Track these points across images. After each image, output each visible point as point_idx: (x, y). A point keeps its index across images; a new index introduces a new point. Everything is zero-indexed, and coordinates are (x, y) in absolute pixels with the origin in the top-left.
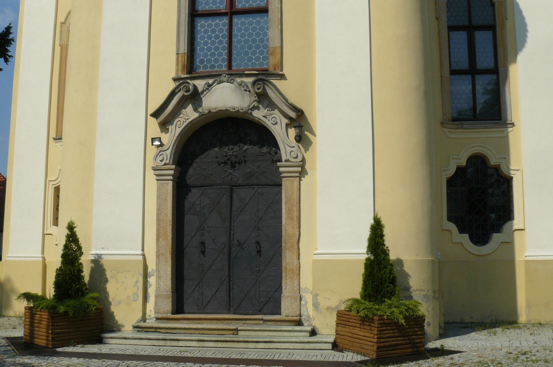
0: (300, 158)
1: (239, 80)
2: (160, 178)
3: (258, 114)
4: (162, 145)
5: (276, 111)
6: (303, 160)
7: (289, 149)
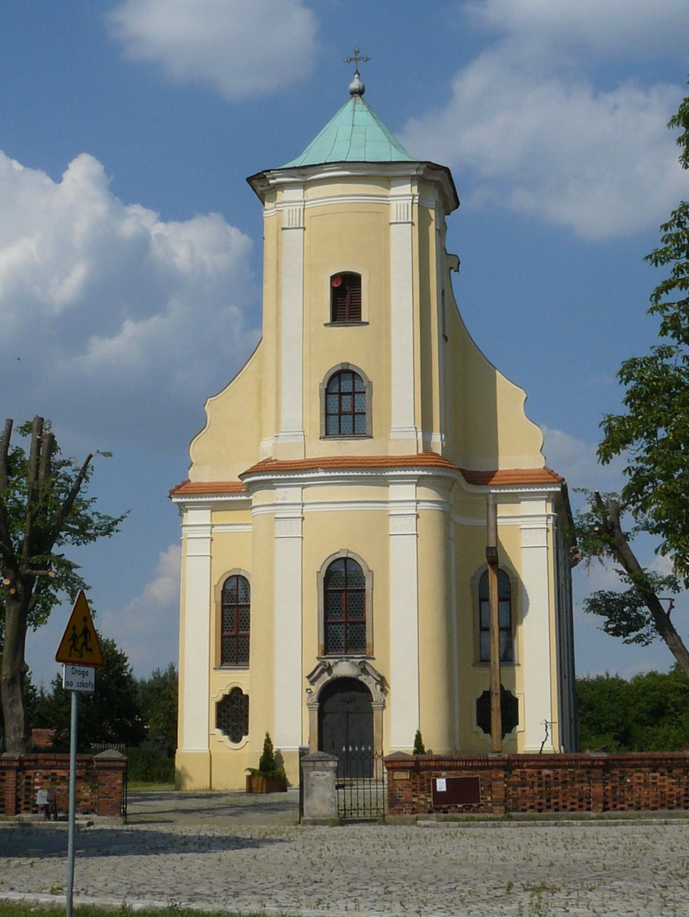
0: (383, 700)
1: (351, 660)
2: (310, 709)
3: (361, 678)
4: (312, 692)
5: (370, 676)
6: (384, 701)
7: (377, 696)
